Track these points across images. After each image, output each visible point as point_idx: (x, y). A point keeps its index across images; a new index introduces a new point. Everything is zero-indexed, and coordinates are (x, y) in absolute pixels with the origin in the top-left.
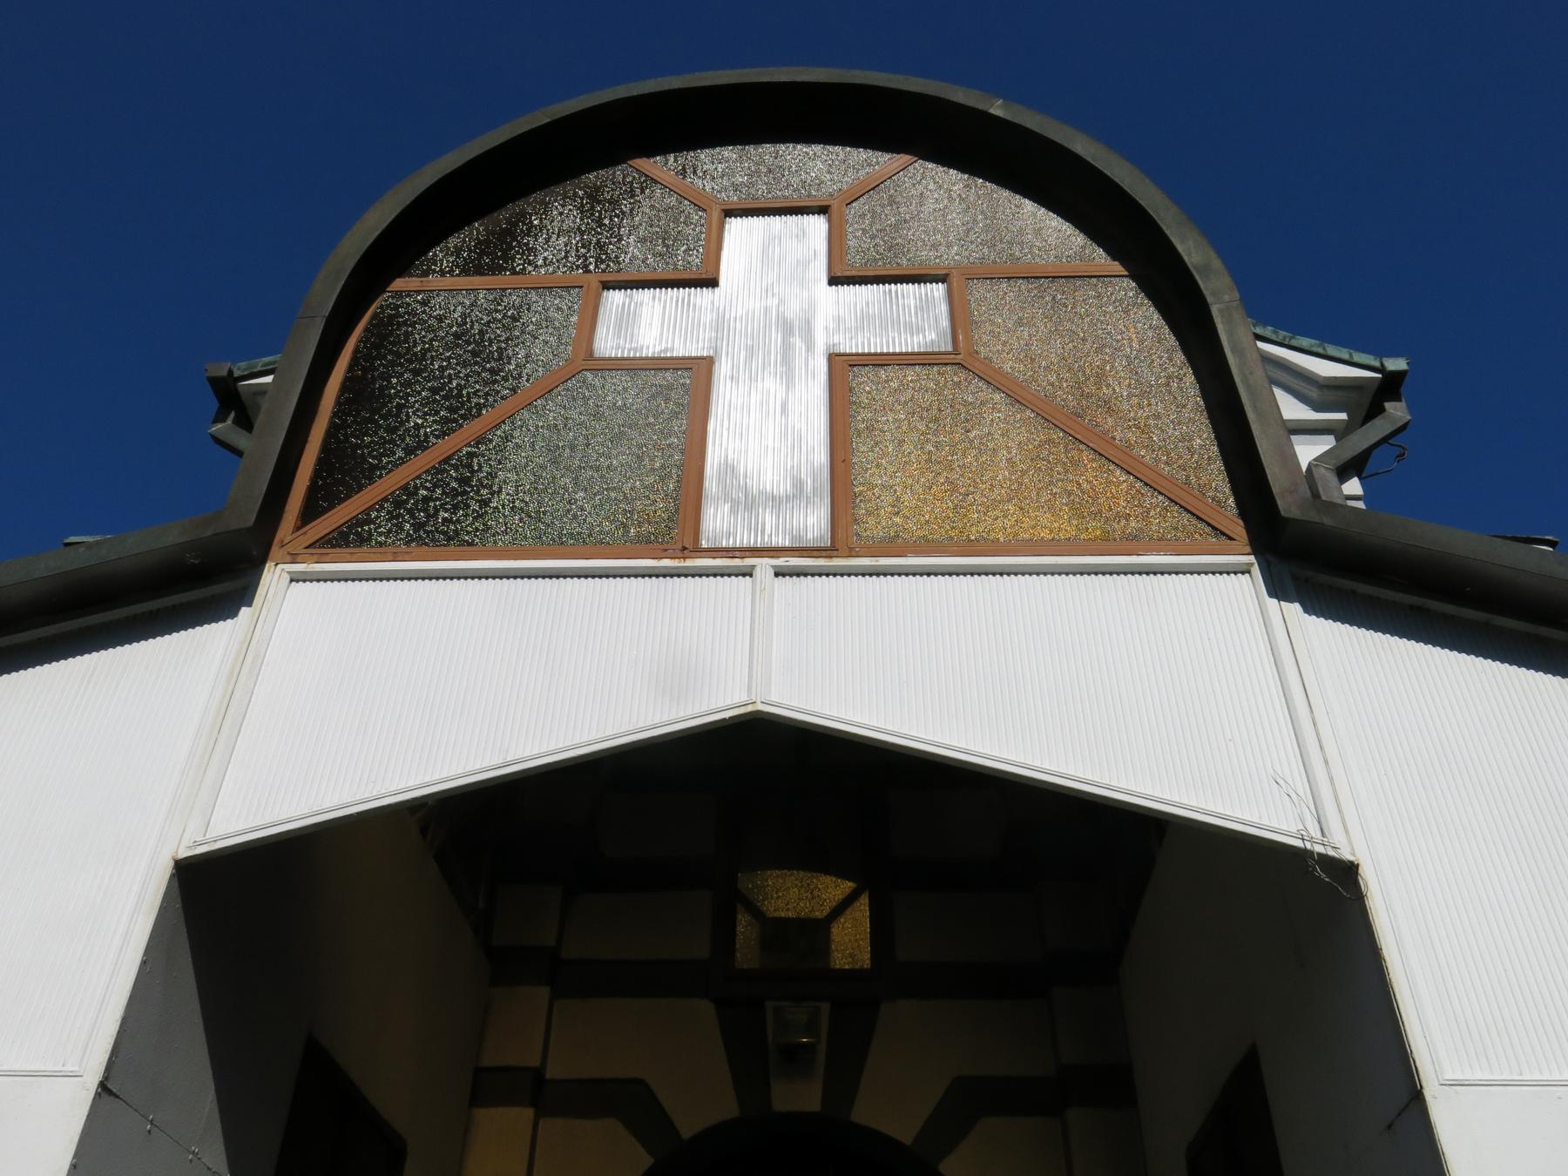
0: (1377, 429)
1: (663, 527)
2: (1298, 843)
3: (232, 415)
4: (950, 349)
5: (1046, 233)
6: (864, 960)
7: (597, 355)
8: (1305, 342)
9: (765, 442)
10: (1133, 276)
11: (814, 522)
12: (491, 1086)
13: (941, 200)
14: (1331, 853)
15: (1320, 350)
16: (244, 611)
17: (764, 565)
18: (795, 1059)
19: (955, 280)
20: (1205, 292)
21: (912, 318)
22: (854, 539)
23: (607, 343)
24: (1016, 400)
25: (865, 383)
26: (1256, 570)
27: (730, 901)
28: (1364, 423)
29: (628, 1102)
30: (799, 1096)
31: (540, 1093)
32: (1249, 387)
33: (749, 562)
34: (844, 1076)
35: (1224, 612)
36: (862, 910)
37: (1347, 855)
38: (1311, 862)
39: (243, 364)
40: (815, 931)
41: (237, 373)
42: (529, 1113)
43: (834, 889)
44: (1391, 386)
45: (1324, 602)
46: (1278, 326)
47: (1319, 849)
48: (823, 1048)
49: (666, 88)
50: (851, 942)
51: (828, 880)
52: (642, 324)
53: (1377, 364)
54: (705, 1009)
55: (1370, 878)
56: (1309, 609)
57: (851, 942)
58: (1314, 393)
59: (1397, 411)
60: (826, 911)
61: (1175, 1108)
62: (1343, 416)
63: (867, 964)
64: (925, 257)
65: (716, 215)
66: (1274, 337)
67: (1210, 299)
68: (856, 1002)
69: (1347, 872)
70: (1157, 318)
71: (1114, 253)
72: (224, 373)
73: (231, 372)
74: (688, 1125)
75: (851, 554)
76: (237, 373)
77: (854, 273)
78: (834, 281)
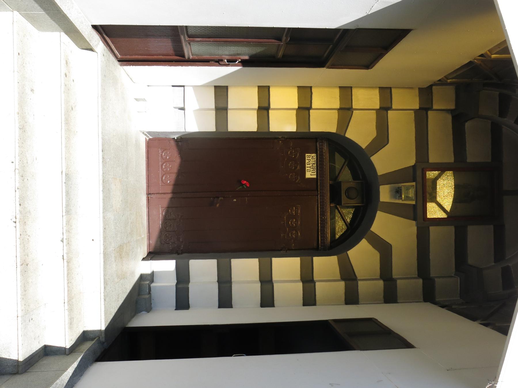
6: (429, 216)
12: (386, 93)
18: (398, 192)
27: (442, 168)
29: (382, 139)
30: (385, 194)
31: (385, 108)
35: (19, 243)
38: (493, 383)
42: (378, 107)
43: (448, 204)
48: (400, 201)
50: (433, 212)
54: (412, 162)
61: (389, 316)
63: (428, 217)
68: (416, 212)
74: (374, 159)
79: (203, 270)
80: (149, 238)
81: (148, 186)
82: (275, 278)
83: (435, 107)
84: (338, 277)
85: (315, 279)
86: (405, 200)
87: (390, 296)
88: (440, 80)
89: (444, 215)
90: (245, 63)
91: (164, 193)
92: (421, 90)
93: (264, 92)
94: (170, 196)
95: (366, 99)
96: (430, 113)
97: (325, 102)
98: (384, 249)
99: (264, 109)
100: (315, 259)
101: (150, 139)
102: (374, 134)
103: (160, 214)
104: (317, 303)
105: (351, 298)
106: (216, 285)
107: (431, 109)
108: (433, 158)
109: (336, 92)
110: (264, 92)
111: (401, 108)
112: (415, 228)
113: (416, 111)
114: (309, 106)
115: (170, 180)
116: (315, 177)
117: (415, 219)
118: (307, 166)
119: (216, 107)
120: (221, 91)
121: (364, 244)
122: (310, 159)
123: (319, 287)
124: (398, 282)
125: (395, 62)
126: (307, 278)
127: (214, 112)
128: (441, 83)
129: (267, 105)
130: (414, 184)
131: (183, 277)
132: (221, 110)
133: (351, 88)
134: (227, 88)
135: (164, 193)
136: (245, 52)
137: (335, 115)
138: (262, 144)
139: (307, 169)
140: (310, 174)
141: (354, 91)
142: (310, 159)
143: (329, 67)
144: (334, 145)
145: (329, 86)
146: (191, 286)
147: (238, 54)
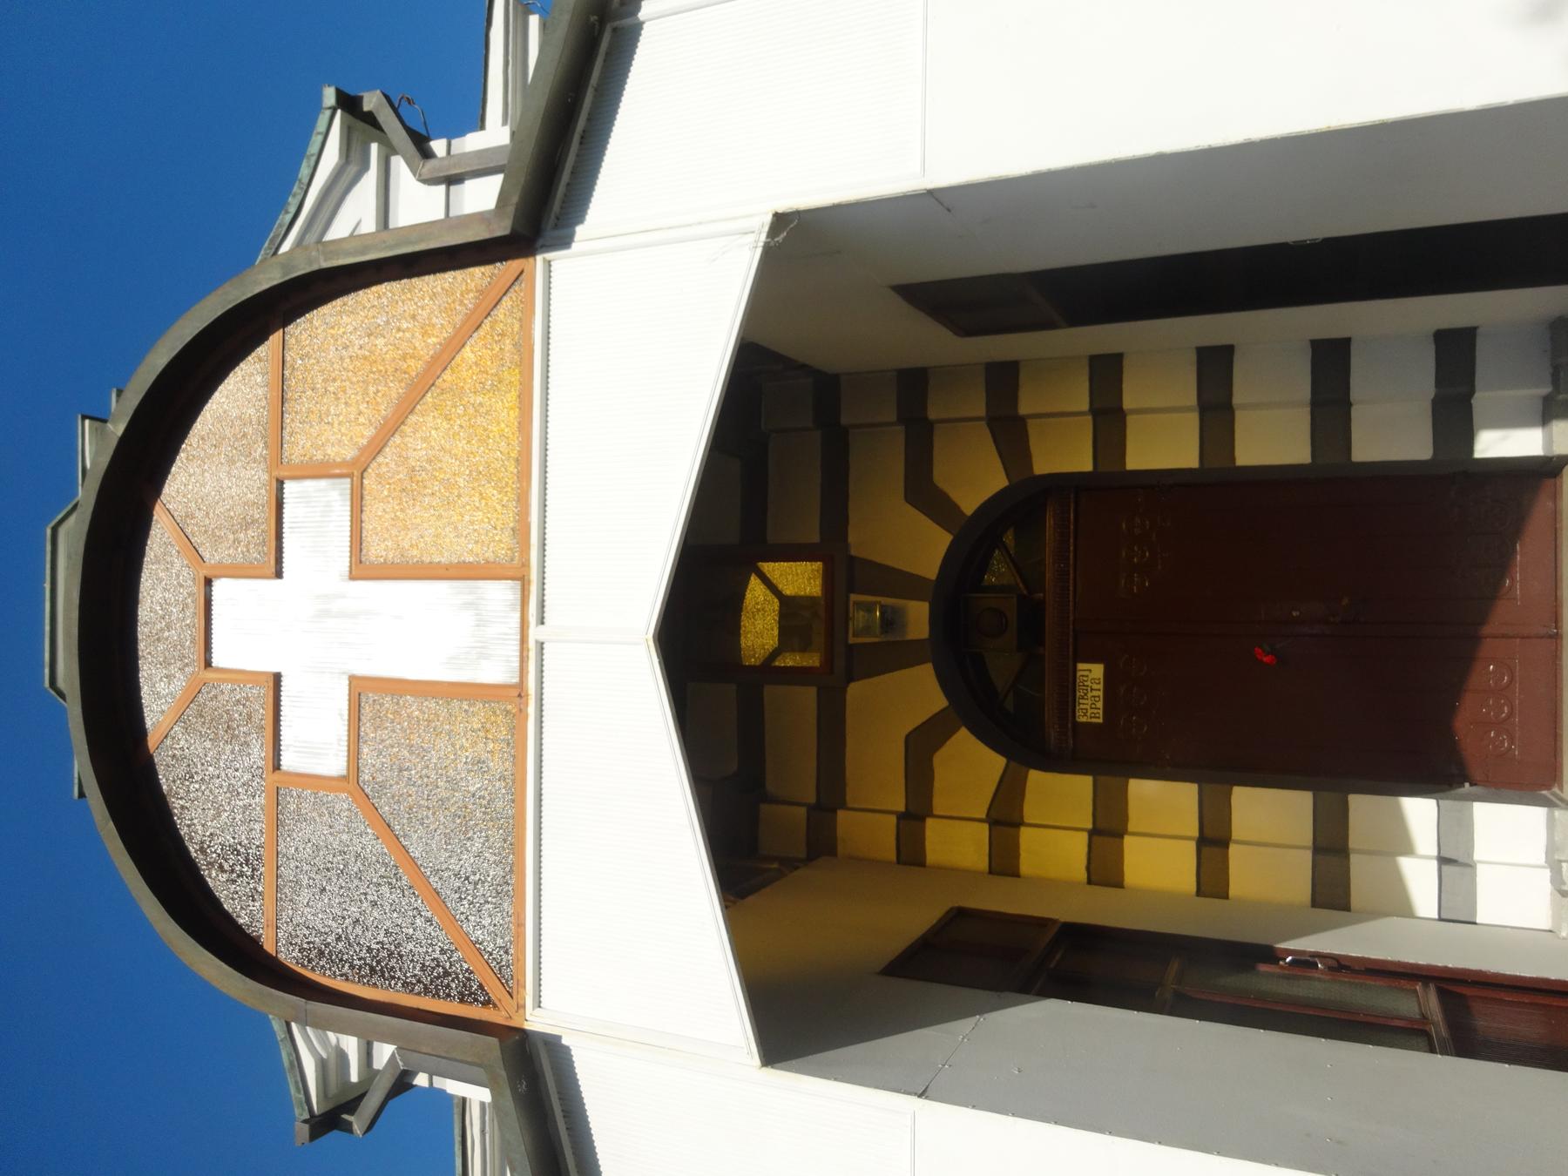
0: (386, 117)
1: (510, 707)
2: (759, 251)
3: (345, 1116)
4: (348, 480)
5: (238, 396)
7: (344, 772)
8: (304, 171)
9: (440, 633)
10: (285, 324)
11: (500, 594)
12: (911, 852)
13: (206, 477)
14: (766, 229)
15: (313, 159)
16: (564, 1041)
17: (534, 633)
18: (891, 621)
19: (282, 474)
20: (308, 270)
21: (317, 513)
22: (517, 567)
23: (334, 763)
24: (395, 430)
25: (376, 550)
26: (549, 256)
27: (768, 670)
28: (380, 128)
29: (922, 747)
30: (918, 618)
31: (915, 816)
32: (397, 245)
33: (532, 645)
34: (908, 585)
36: (771, 568)
37: (768, 219)
39: (297, 1111)
40: (790, 608)
41: (306, 1116)
42: (930, 822)
43: (755, 591)
44: (349, 103)
45: (575, 207)
46: (288, 191)
47: (763, 237)
49: (80, 720)
50: (801, 578)
51: (748, 595)
52: (315, 739)
53: (328, 113)
54: (855, 690)
55: (785, 205)
56: (580, 218)
57: (801, 578)
58: (352, 169)
59: (371, 101)
60: (770, 596)
61: (932, 343)
62: (374, 147)
63: (818, 565)
64: (265, 496)
65: (209, 675)
66: (299, 198)
67: (315, 267)
68: (847, 573)
69: (781, 221)
70: (325, 309)
71: (261, 338)
72: (306, 1127)
73: (305, 1121)
74: (939, 702)
75: (526, 565)
76: (306, 1116)
77: (273, 562)
78: (279, 574)
79: (1392, 431)
80: (1555, 516)
81: (1556, 657)
82: (1193, 419)
83: (803, 811)
84: (1033, 427)
85: (1090, 418)
86: (875, 603)
87: (913, 385)
88: (797, 868)
89: (768, 567)
90: (1269, 955)
91: (1504, 636)
92: (831, 850)
93: (1212, 878)
94: (1486, 630)
95: (958, 843)
96: (812, 800)
97: (1055, 847)
98: (925, 494)
99: (1213, 841)
100: (1087, 465)
101: (1548, 787)
102: (938, 758)
103: (1520, 582)
104: (1086, 363)
105: (1003, 380)
106: (1355, 394)
107: (811, 809)
108: (808, 697)
109: (1026, 865)
110: (1212, 878)
111: (878, 816)
112: (851, 539)
113: (844, 806)
114: (1096, 839)
115: (1488, 671)
116: (1081, 666)
117: (852, 559)
118: (1101, 693)
119: (1347, 857)
120: (1332, 893)
121: (969, 502)
122: (1091, 707)
123: (1080, 400)
124: (893, 417)
125: (912, 918)
126: (1109, 420)
127: (1353, 843)
128: (790, 864)
129: (1206, 850)
130: (852, 640)
131: (1454, 417)
132: (1331, 846)
133: (990, 872)
134: (1316, 903)
135: (1504, 636)
136: (1265, 980)
137: (1030, 811)
138: (1223, 756)
139: (1101, 686)
140: (1092, 674)
141: (982, 863)
142: (1091, 707)
143: (1053, 921)
144: (1032, 736)
145: (1045, 884)
146: (1431, 391)
147: (1287, 977)
